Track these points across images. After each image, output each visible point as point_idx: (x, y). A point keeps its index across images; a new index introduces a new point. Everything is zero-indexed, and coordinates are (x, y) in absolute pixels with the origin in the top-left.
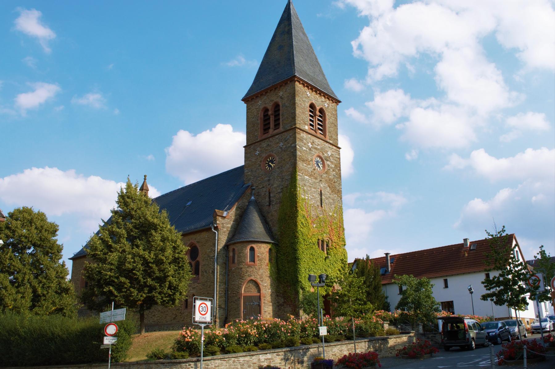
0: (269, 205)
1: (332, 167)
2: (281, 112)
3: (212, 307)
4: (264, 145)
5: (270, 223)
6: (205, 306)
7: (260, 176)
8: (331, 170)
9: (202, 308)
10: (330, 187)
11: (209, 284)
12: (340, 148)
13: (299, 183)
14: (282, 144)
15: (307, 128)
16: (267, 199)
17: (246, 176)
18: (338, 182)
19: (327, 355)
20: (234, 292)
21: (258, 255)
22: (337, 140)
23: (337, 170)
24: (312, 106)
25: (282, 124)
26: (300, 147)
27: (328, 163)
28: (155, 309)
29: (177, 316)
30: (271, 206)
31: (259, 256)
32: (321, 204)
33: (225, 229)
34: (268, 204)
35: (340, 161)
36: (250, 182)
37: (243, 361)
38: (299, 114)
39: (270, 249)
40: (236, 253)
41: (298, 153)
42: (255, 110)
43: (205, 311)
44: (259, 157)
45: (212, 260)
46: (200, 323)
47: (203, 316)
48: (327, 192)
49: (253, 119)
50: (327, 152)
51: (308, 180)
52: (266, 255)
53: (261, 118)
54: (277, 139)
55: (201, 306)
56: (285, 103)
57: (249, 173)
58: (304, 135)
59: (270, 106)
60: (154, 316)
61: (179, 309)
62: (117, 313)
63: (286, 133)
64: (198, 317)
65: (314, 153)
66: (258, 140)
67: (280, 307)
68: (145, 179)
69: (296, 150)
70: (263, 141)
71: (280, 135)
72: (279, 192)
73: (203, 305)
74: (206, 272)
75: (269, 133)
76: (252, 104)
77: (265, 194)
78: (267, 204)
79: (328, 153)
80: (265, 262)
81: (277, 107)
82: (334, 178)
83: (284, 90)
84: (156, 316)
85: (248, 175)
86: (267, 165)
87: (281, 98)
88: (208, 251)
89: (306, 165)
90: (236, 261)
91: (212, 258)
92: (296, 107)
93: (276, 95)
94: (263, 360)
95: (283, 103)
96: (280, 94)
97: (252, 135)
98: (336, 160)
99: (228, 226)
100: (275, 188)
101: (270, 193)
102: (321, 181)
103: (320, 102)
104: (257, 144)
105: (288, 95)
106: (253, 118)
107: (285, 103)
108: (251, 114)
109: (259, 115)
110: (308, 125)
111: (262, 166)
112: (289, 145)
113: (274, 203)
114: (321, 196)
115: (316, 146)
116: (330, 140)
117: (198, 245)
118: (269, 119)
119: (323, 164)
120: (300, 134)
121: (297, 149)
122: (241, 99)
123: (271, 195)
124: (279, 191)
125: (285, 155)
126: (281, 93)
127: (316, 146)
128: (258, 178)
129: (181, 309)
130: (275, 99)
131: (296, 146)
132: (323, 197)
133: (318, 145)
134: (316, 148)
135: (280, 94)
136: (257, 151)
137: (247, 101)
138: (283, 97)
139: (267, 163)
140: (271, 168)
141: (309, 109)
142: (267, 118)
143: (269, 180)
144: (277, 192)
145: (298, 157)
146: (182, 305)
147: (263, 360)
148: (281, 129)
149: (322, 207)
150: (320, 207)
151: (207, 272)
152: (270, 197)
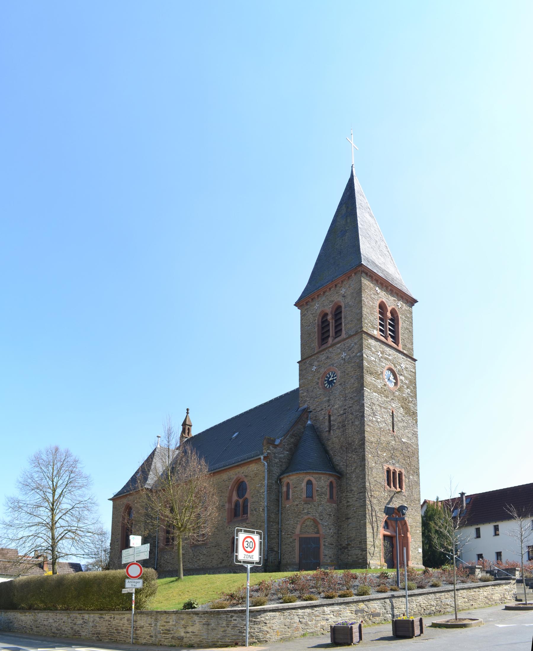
0: (329, 431)
1: (406, 384)
2: (343, 315)
3: (261, 543)
4: (322, 357)
5: (331, 452)
6: (251, 540)
7: (318, 396)
8: (405, 387)
9: (247, 542)
10: (403, 408)
11: (259, 524)
12: (415, 360)
13: (367, 403)
14: (345, 355)
15: (376, 333)
16: (327, 423)
17: (301, 397)
18: (413, 402)
19: (410, 606)
20: (289, 533)
21: (317, 489)
22: (412, 349)
23: (411, 387)
24: (382, 307)
25: (345, 329)
26: (367, 356)
27: (402, 378)
28: (199, 552)
29: (223, 560)
30: (332, 431)
31: (318, 490)
32: (393, 429)
33: (277, 460)
34: (327, 429)
35: (415, 376)
36: (306, 404)
37: (303, 612)
38: (366, 315)
39: (331, 483)
40: (290, 487)
41: (365, 364)
42: (311, 316)
43: (251, 547)
44: (316, 373)
45: (263, 496)
46: (244, 562)
47: (248, 554)
48: (400, 413)
49: (309, 328)
50: (400, 364)
51: (377, 397)
52: (327, 489)
53: (318, 325)
54: (338, 348)
55: (246, 540)
56: (348, 303)
57: (305, 394)
58: (372, 342)
59: (328, 309)
60: (199, 560)
61: (226, 553)
62: (140, 551)
63: (349, 340)
64: (242, 555)
65: (384, 365)
66: (315, 352)
67: (343, 550)
68: (188, 413)
69: (362, 360)
70: (322, 353)
71: (342, 343)
72: (342, 415)
73: (249, 540)
74: (255, 510)
75: (328, 343)
76: (307, 309)
77: (324, 418)
78: (326, 430)
79: (402, 366)
80: (326, 497)
81: (338, 312)
82: (408, 397)
83: (347, 286)
84: (201, 560)
85: (304, 396)
86: (326, 382)
87: (344, 296)
88: (258, 485)
89: (374, 379)
90: (291, 497)
91: (262, 494)
92: (363, 305)
93: (337, 293)
94: (329, 612)
95: (346, 302)
96: (341, 292)
97: (308, 347)
98: (410, 375)
99: (280, 456)
100: (336, 409)
101: (330, 416)
102: (393, 399)
103: (391, 302)
104: (313, 357)
105: (352, 291)
106: (309, 326)
107: (348, 303)
108: (306, 321)
109: (316, 321)
110: (377, 330)
111: (320, 384)
112: (354, 354)
113: (335, 428)
114: (393, 419)
115: (387, 356)
116: (403, 349)
117: (246, 480)
118: (329, 325)
119: (395, 378)
120: (368, 340)
121: (364, 359)
122: (294, 304)
123: (332, 418)
124: (342, 412)
125: (348, 367)
126: (344, 290)
127: (387, 356)
128: (316, 399)
129: (228, 552)
130: (337, 299)
131: (362, 355)
132: (395, 419)
133: (389, 355)
134: (386, 359)
135: (341, 292)
136: (314, 366)
137: (301, 306)
138: (345, 295)
139: (326, 380)
140: (331, 386)
141: (378, 309)
142: (326, 324)
143: (329, 400)
144: (339, 414)
145: (365, 368)
146: (229, 547)
147: (329, 612)
148: (344, 335)
149: (393, 431)
150: (391, 432)
151: (257, 510)
152: (330, 421)
